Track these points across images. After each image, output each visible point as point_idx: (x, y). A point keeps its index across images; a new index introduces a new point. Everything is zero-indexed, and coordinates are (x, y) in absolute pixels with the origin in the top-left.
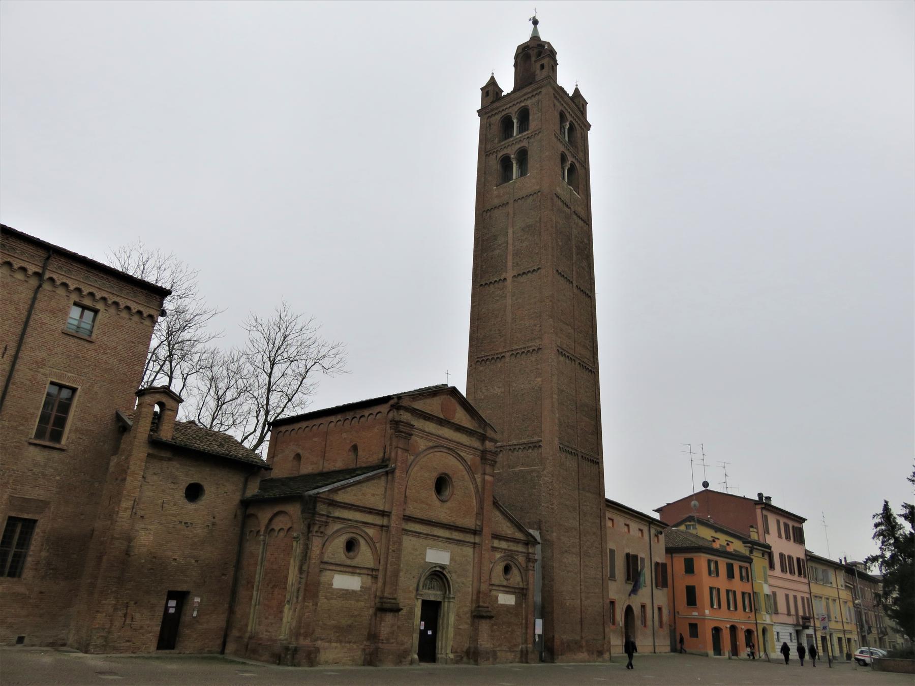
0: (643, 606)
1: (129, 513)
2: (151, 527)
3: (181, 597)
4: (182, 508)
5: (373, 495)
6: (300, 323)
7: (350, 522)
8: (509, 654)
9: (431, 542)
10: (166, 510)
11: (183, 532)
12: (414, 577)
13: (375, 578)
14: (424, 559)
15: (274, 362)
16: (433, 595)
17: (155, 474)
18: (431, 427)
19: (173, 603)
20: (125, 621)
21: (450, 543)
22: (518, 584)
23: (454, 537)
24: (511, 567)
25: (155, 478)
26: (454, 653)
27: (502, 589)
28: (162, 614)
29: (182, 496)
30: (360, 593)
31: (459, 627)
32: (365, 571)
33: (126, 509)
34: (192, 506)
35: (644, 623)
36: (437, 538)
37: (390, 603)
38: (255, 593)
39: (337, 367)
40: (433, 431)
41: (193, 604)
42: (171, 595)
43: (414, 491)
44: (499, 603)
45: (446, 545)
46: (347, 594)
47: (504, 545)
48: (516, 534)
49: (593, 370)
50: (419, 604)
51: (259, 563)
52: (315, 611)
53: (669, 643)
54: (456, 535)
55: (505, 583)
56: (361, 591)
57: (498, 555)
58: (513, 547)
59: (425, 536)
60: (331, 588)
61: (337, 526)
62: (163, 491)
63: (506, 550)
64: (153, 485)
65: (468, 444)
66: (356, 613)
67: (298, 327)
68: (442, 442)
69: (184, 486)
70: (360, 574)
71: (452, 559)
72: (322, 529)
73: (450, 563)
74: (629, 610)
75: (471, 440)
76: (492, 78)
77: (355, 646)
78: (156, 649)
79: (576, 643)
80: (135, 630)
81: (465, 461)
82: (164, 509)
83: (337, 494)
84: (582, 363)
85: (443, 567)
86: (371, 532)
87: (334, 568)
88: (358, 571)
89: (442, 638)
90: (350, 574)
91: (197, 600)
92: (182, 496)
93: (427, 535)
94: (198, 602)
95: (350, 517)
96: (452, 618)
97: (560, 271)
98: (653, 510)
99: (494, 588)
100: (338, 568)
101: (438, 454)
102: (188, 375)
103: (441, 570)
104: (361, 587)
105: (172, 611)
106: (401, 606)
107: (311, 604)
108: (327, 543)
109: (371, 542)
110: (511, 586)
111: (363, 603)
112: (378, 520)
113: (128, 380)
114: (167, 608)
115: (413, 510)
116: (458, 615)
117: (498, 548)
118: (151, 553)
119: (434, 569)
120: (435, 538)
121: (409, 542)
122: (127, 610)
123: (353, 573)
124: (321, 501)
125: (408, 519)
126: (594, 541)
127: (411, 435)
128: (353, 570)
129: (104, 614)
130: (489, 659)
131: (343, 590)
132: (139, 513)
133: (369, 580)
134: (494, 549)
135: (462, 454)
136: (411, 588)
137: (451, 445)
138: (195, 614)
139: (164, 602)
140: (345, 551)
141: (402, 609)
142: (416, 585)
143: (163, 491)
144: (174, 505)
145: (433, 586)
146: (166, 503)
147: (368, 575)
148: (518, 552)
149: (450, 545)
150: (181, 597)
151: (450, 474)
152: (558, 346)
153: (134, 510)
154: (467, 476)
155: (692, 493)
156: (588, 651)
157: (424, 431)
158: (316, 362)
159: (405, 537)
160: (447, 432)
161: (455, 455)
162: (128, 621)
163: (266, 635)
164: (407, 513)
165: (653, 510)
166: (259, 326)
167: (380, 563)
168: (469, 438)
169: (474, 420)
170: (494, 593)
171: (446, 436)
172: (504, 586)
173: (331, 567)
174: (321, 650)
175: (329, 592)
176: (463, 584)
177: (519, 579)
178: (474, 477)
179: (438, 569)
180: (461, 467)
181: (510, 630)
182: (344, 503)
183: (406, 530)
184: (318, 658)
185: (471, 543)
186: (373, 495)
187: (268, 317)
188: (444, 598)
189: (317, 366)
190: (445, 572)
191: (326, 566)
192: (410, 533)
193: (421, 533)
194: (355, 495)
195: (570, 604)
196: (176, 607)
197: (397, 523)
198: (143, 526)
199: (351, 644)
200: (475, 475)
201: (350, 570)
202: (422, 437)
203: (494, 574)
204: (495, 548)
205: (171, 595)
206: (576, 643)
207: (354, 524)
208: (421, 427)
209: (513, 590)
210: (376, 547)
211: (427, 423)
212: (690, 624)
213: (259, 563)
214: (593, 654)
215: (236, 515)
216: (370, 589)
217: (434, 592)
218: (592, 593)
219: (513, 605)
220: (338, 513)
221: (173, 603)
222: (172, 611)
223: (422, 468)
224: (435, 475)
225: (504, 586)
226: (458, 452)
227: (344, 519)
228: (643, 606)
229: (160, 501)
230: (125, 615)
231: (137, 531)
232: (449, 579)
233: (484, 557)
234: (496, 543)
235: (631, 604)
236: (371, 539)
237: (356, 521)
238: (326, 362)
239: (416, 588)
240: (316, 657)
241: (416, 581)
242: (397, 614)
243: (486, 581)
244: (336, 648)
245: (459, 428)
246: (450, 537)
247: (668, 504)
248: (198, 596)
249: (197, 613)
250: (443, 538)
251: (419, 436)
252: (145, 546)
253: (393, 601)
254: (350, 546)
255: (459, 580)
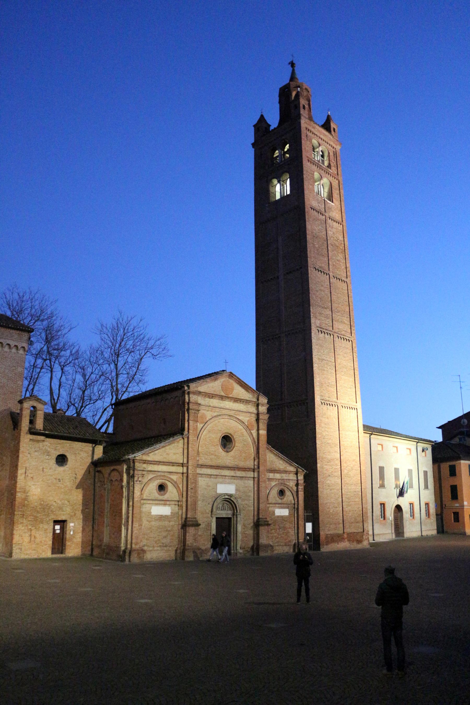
0: (411, 504)
1: (24, 476)
2: (38, 483)
3: (62, 523)
4: (55, 470)
5: (175, 454)
6: (134, 323)
7: (159, 473)
8: (285, 547)
9: (221, 480)
10: (46, 472)
11: (58, 485)
12: (209, 504)
13: (180, 506)
14: (216, 492)
15: (118, 353)
16: (226, 513)
17: (36, 451)
18: (215, 402)
19: (57, 527)
20: (31, 539)
21: (234, 479)
22: (291, 501)
23: (248, 476)
24: (284, 491)
25: (36, 453)
26: (243, 549)
27: (277, 505)
28: (52, 534)
29: (54, 463)
30: (171, 517)
31: (246, 533)
32: (173, 503)
33: (21, 474)
34: (61, 469)
35: (412, 515)
36: (224, 477)
37: (191, 521)
38: (105, 519)
39: (163, 353)
40: (216, 405)
41: (70, 527)
42: (56, 522)
43: (205, 447)
44: (276, 515)
45: (232, 481)
46: (161, 518)
47: (278, 476)
48: (288, 468)
49: (350, 339)
50: (214, 520)
51: (106, 501)
52: (140, 529)
53: (436, 528)
54: (239, 474)
55: (280, 501)
56: (171, 515)
57: (273, 484)
58: (285, 476)
59: (215, 477)
60: (150, 515)
61: (151, 476)
62: (42, 461)
63: (279, 479)
64: (35, 458)
65: (245, 410)
66: (169, 529)
67: (132, 327)
68: (224, 412)
69: (55, 457)
70: (169, 505)
71: (237, 490)
72: (140, 479)
73: (236, 492)
74: (398, 508)
75: (247, 407)
76: (262, 116)
77: (170, 549)
78: (51, 554)
79: (338, 537)
80: (38, 544)
81: (243, 422)
82: (44, 472)
83: (77, 488)
84: (339, 336)
85: (231, 495)
86: (174, 477)
87: (151, 502)
88: (168, 503)
89: (233, 541)
90: (163, 505)
91: (72, 524)
92: (54, 463)
93: (217, 475)
94: (72, 526)
95: (160, 470)
96: (240, 528)
97: (317, 268)
98: (437, 428)
99: (271, 505)
100: (154, 502)
101: (222, 420)
102: (64, 366)
103: (229, 497)
104: (171, 513)
105: (58, 532)
106: (200, 522)
107: (137, 525)
108: (145, 488)
109: (175, 484)
110: (285, 503)
111: (173, 523)
112: (180, 469)
113: (14, 391)
114: (54, 530)
115: (203, 460)
116: (244, 525)
117: (273, 479)
118: (40, 499)
119: (224, 497)
120: (223, 477)
121: (202, 482)
122: (31, 532)
123: (165, 505)
124: (138, 462)
125: (202, 466)
126: (353, 466)
127: (199, 411)
128: (165, 502)
129: (18, 535)
130: (268, 552)
131: (159, 515)
132: (29, 476)
133: (176, 508)
134: (270, 480)
135: (240, 418)
136: (207, 511)
137: (232, 413)
138: (72, 533)
139: (52, 527)
140: (158, 492)
141: (200, 525)
142: (210, 509)
143: (42, 461)
144: (50, 469)
145: (224, 508)
146: (45, 469)
147: (175, 505)
148: (289, 480)
149: (235, 481)
150: (62, 523)
151: (231, 432)
152: (317, 327)
153: (26, 474)
154: (245, 433)
155: (461, 414)
156: (349, 540)
157: (210, 406)
158: (147, 352)
159: (200, 478)
160: (228, 404)
161: (235, 419)
162: (33, 539)
163: (114, 544)
164: (200, 463)
165: (437, 428)
166: (105, 330)
167: (183, 497)
168: (245, 406)
169: (249, 392)
170: (270, 509)
171: (228, 407)
172: (279, 504)
173: (149, 502)
174: (147, 552)
175: (149, 518)
176: (246, 505)
177: (291, 498)
178: (251, 432)
179: (227, 497)
180: (241, 427)
181: (285, 531)
182: (154, 461)
183: (200, 474)
184: (145, 557)
185: (251, 478)
186: (175, 454)
187: (110, 322)
188: (233, 515)
189: (148, 354)
190: (232, 499)
191: (145, 502)
192: (204, 476)
193: (212, 475)
194: (161, 455)
195: (333, 511)
196: (60, 529)
197: (193, 470)
198: (33, 483)
199: (168, 548)
200: (251, 431)
201: (163, 502)
202: (208, 411)
203: (271, 496)
204: (271, 479)
205: (56, 522)
206: (338, 537)
207: (163, 474)
208: (207, 404)
209: (287, 506)
210: (179, 487)
211: (212, 400)
212: (454, 513)
213: (106, 501)
214: (353, 542)
215: (89, 472)
216: (178, 513)
217: (225, 512)
218: (353, 502)
219: (287, 516)
220: (151, 467)
221: (57, 527)
222: (58, 532)
223: (209, 432)
224: (219, 436)
225: (279, 504)
226: (237, 417)
227: (155, 471)
228: (411, 504)
229: (41, 467)
230: (31, 535)
231: (30, 486)
232: (236, 503)
233: (262, 487)
234: (271, 475)
235: (399, 504)
236: (176, 482)
237: (164, 472)
238: (154, 351)
239: (211, 511)
240: (144, 556)
241: (211, 506)
242: (197, 528)
243: (264, 502)
244: (157, 550)
245: (237, 400)
246: (235, 475)
247: (449, 422)
248: (73, 522)
249: (73, 532)
250: (229, 476)
251: (206, 410)
252: (35, 495)
253: (194, 519)
254: (162, 488)
255: (243, 503)
